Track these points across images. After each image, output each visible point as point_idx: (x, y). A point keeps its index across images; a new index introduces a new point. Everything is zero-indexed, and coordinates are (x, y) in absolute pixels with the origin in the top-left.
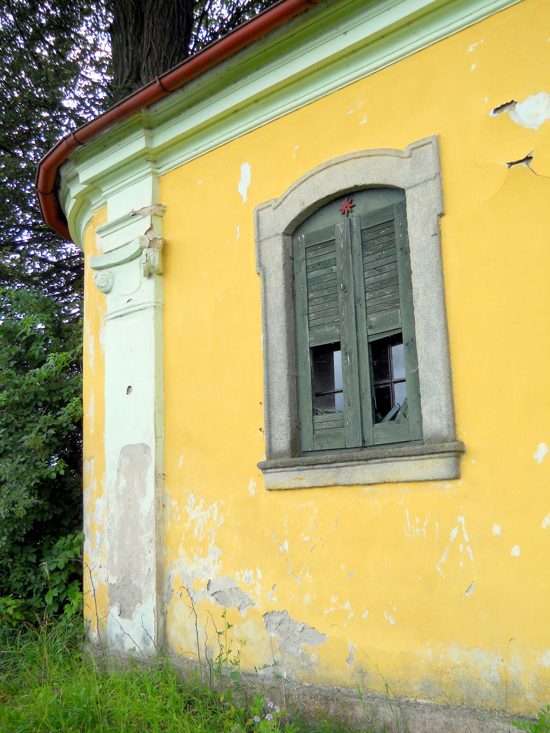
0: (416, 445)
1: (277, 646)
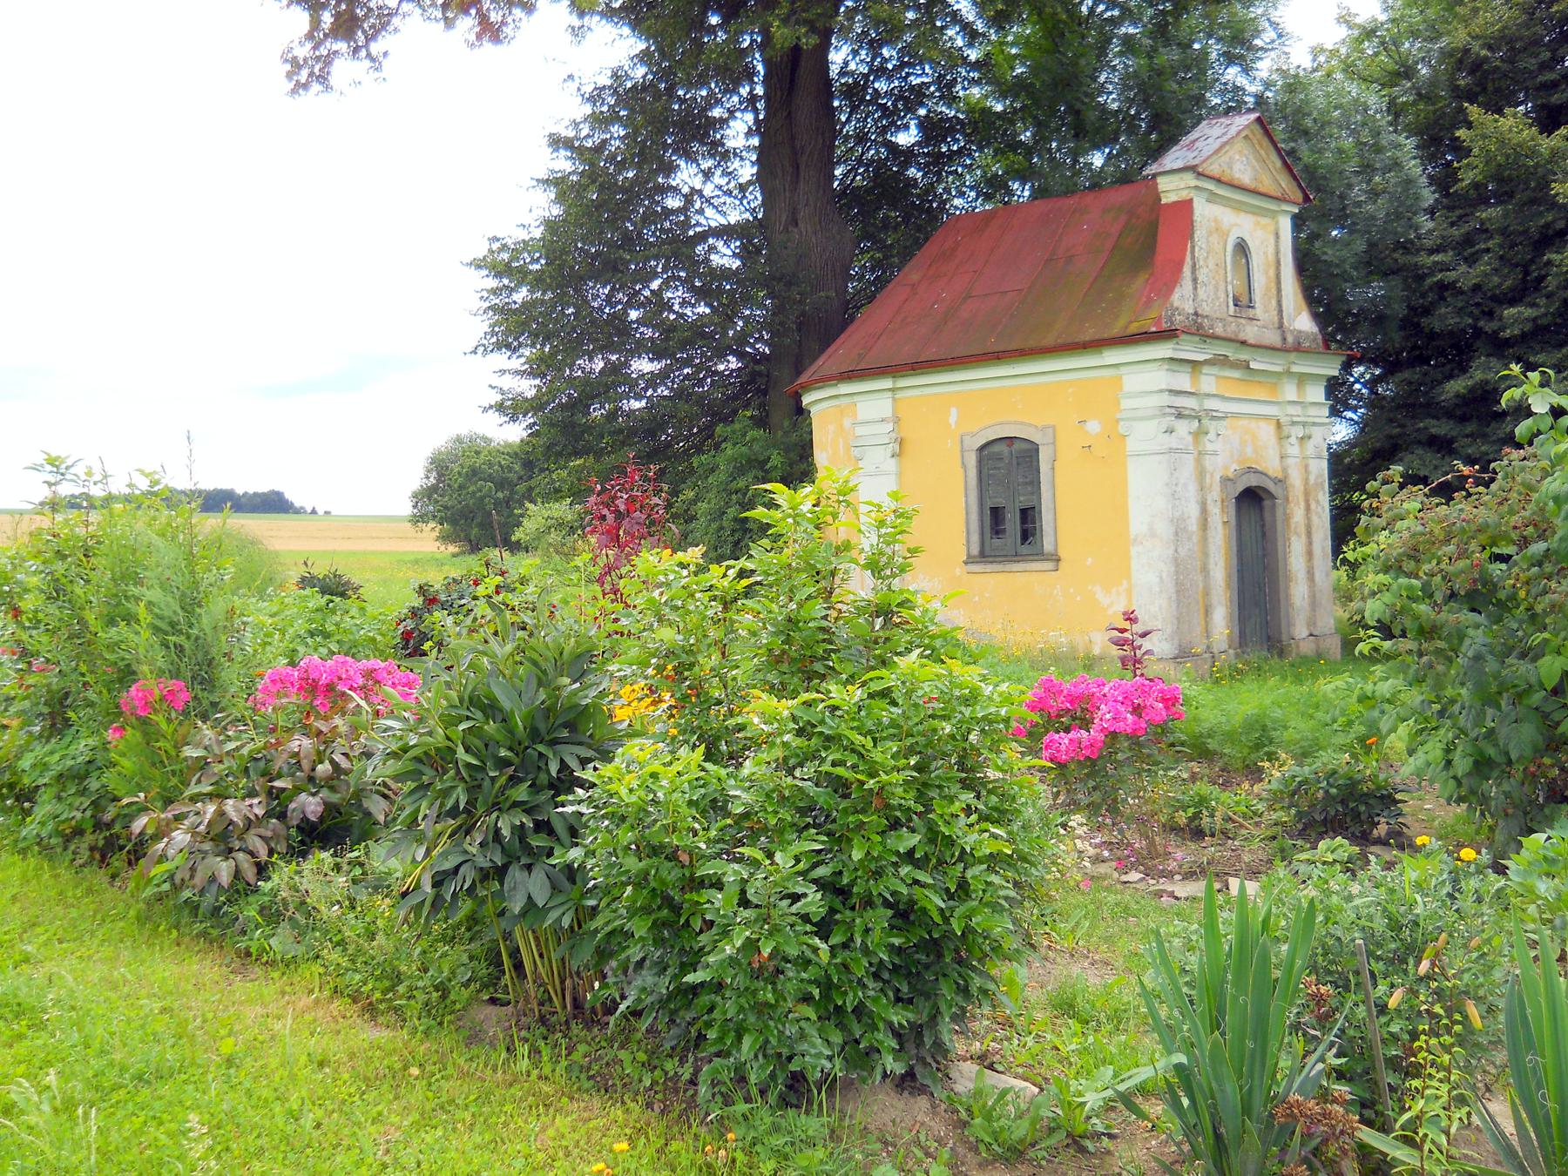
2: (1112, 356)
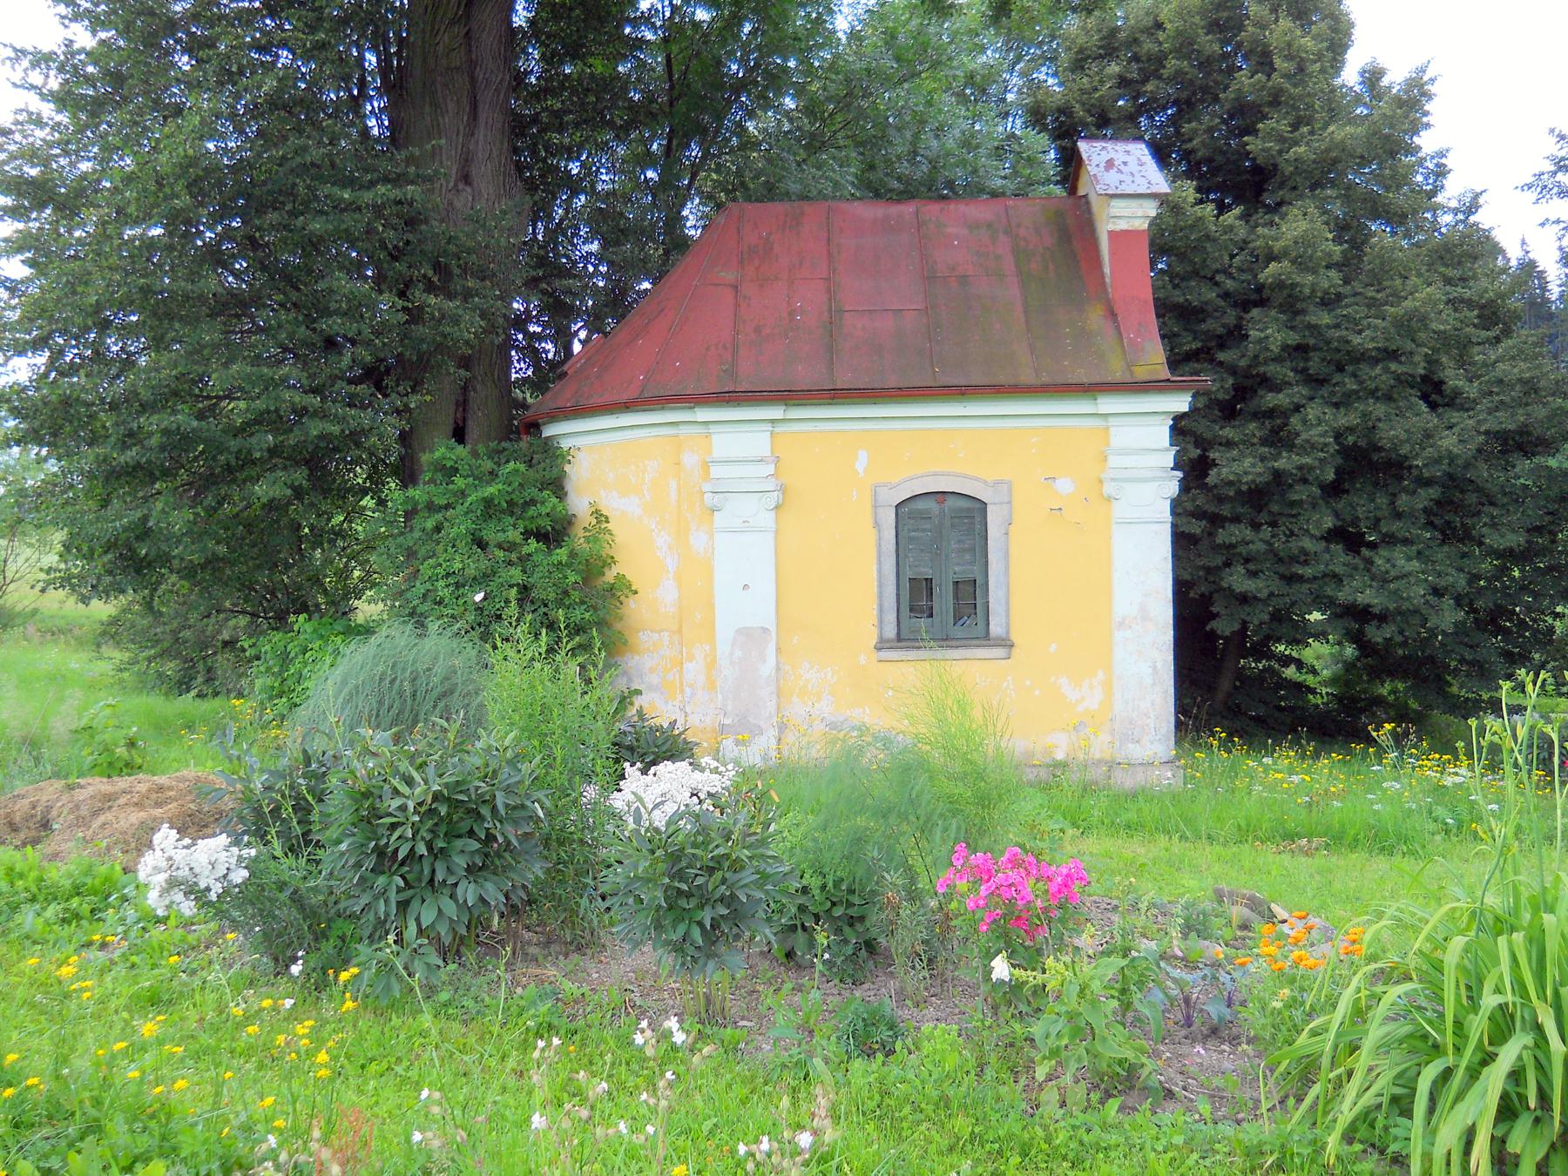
0: (985, 638)
1: (1404, 427)
2: (1109, 404)
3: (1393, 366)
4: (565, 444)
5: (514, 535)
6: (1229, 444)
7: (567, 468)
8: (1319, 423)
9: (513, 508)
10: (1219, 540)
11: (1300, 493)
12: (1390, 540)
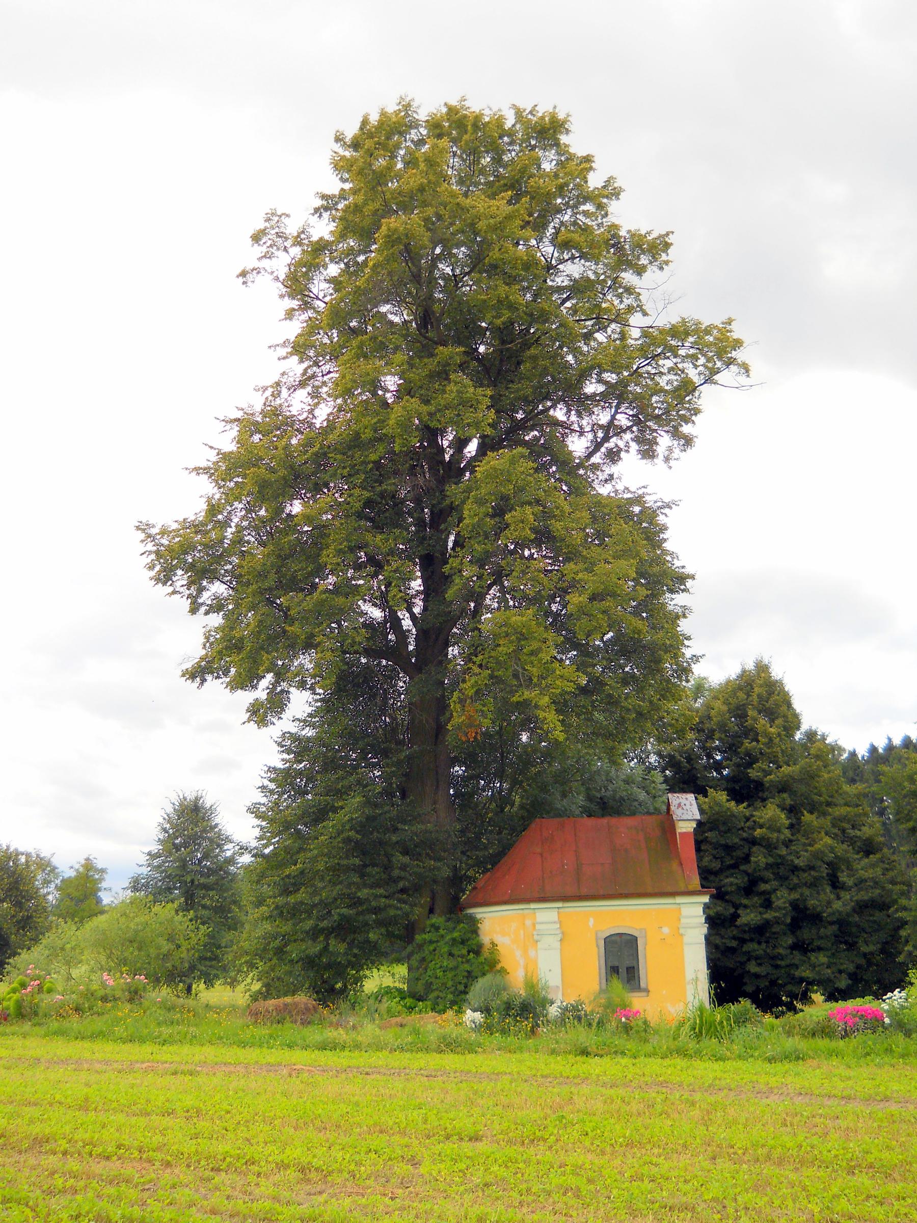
2: (679, 900)
3: (813, 873)
4: (478, 916)
5: (464, 952)
6: (746, 907)
7: (479, 925)
8: (783, 898)
9: (463, 942)
10: (744, 950)
11: (776, 929)
12: (819, 949)
